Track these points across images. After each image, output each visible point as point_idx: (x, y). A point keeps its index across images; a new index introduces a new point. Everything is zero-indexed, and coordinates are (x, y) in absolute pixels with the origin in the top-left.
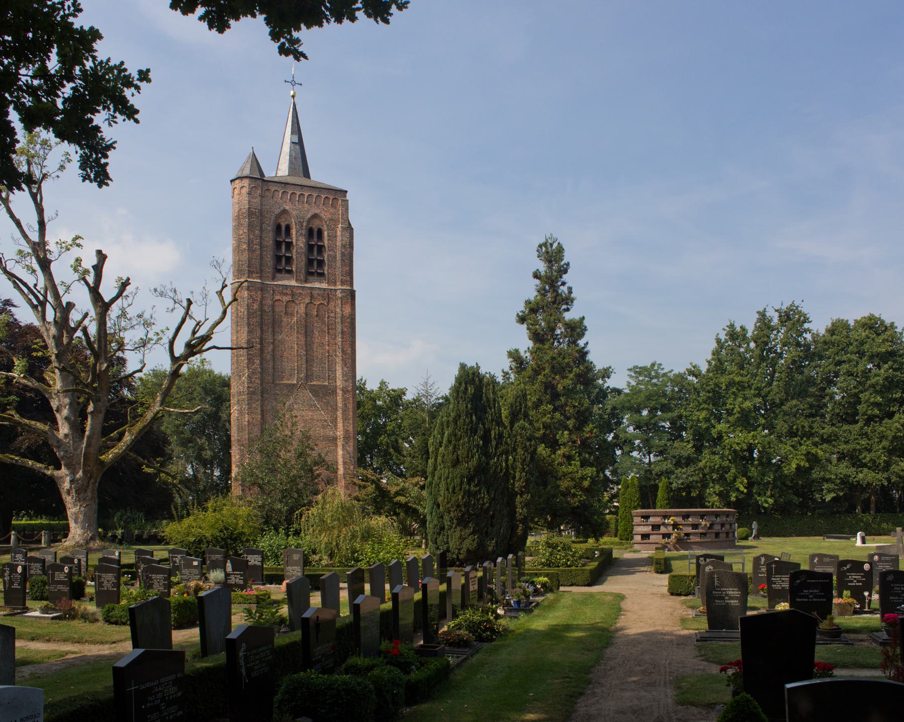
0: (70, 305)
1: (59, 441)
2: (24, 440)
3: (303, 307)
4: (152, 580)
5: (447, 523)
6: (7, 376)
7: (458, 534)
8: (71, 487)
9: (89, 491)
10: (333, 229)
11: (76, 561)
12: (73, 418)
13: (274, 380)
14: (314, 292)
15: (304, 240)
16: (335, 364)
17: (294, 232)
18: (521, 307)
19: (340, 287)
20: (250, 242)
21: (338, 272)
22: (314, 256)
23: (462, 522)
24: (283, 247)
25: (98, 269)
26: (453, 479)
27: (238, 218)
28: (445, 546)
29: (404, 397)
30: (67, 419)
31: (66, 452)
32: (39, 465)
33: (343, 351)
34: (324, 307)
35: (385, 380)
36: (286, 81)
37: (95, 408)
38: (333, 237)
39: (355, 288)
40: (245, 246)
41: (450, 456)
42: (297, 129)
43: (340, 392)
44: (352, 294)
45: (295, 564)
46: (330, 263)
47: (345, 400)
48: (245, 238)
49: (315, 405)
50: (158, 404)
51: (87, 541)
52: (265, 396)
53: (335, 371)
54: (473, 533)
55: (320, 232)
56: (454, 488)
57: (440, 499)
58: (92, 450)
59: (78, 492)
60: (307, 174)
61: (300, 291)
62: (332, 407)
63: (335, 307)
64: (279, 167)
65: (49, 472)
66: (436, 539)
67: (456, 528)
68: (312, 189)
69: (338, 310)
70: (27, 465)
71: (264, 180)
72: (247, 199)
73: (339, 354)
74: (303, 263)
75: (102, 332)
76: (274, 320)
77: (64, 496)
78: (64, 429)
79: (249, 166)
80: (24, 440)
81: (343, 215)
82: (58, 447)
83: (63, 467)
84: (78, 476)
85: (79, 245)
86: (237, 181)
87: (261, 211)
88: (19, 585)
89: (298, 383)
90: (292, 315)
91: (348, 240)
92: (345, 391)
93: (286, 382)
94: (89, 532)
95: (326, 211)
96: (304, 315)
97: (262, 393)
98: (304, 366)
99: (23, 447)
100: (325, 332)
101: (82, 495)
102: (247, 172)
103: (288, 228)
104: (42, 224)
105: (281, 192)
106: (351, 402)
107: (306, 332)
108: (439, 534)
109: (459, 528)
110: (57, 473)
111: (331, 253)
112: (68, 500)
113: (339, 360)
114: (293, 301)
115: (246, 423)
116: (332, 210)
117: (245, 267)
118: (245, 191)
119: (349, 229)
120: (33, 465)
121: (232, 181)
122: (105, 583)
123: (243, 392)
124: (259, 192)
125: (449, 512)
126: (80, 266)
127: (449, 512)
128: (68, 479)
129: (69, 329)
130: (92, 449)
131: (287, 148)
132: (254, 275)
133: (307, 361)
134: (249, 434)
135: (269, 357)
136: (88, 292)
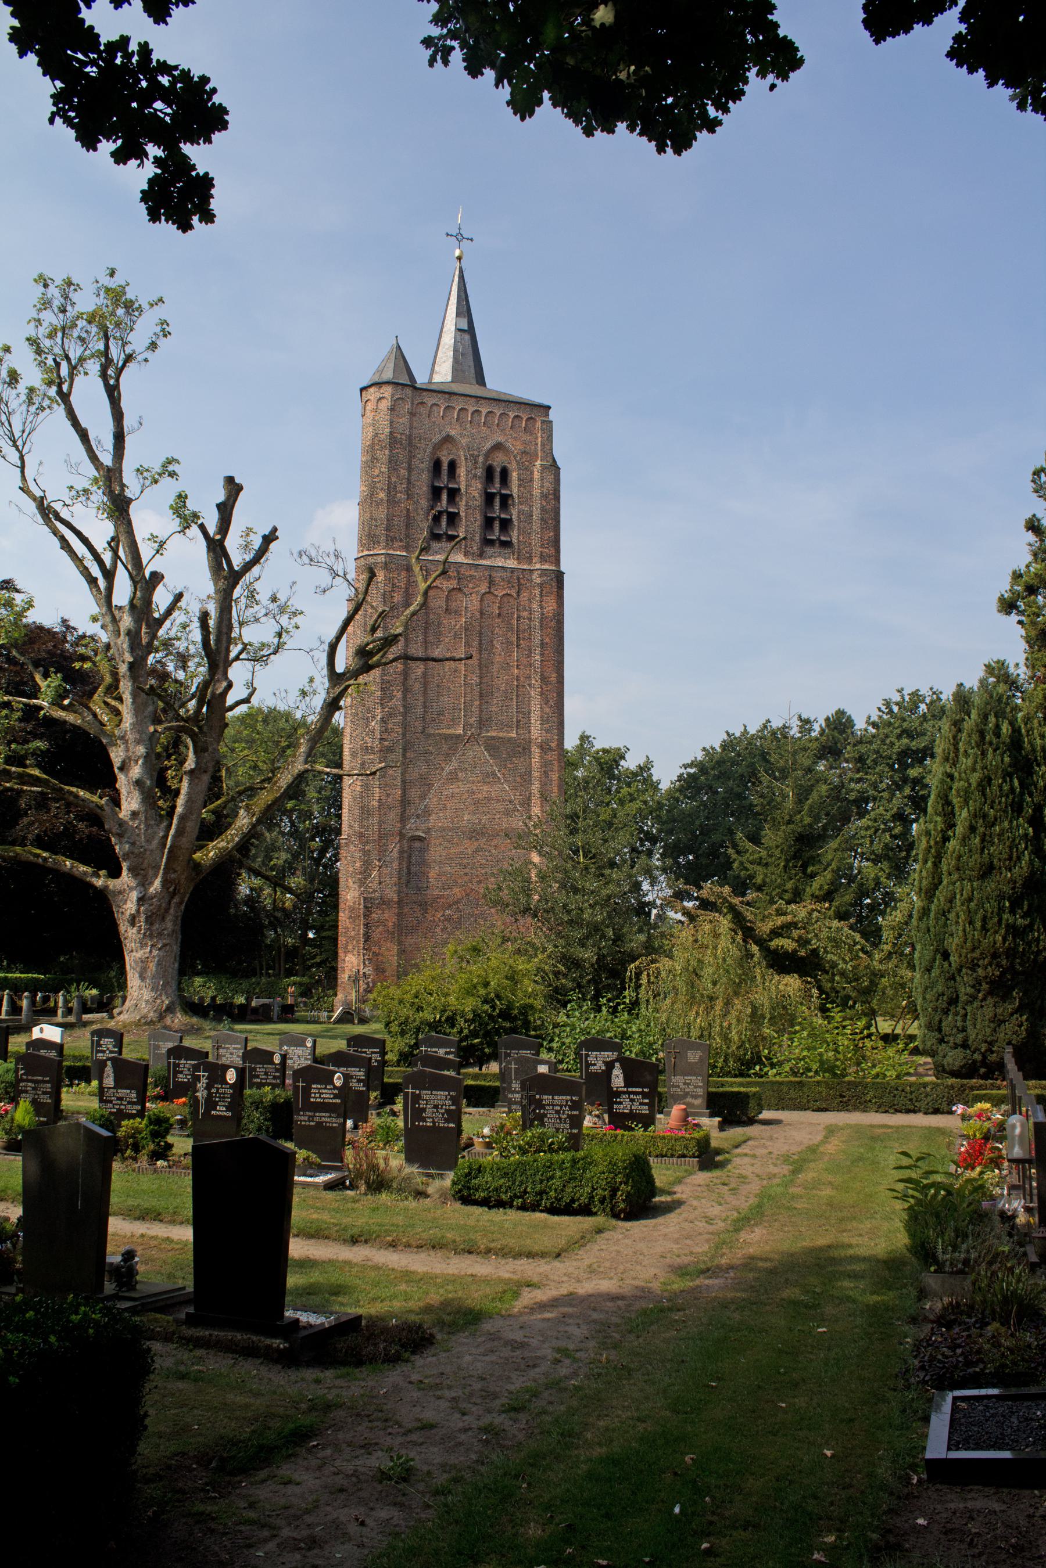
0: (157, 577)
1: (121, 823)
2: (32, 823)
3: (475, 599)
4: (543, 1107)
5: (964, 991)
6: (25, 705)
7: (989, 1012)
8: (138, 911)
9: (169, 918)
10: (526, 469)
11: (277, 1059)
12: (148, 783)
13: (424, 728)
14: (494, 574)
15: (480, 486)
16: (529, 701)
17: (462, 472)
18: (1004, 586)
19: (538, 566)
20: (391, 489)
21: (535, 541)
22: (494, 512)
23: (999, 989)
24: (444, 497)
25: (225, 510)
26: (981, 905)
27: (371, 450)
28: (960, 1036)
29: (622, 763)
30: (138, 783)
31: (133, 844)
32: (83, 868)
33: (543, 678)
34: (512, 600)
35: (587, 733)
36: (448, 235)
37: (197, 763)
38: (526, 482)
39: (562, 569)
40: (382, 495)
41: (977, 856)
42: (465, 309)
43: (536, 751)
44: (559, 578)
45: (690, 1071)
46: (522, 525)
47: (545, 764)
48: (382, 482)
49: (494, 773)
50: (301, 759)
51: (161, 1014)
52: (408, 755)
53: (529, 712)
54: (1019, 1010)
55: (505, 473)
56: (984, 919)
57: (953, 944)
58: (185, 842)
59: (150, 921)
60: (481, 380)
61: (472, 573)
62: (521, 777)
63: (529, 600)
64: (437, 368)
65: (99, 883)
66: (940, 1021)
67: (984, 999)
68: (494, 403)
69: (535, 606)
70: (63, 868)
71: (415, 388)
72: (388, 417)
73: (536, 682)
74: (478, 523)
75: (225, 623)
76: (426, 623)
77: (123, 927)
78: (131, 803)
79: (391, 365)
80: (32, 823)
81: (543, 445)
82: (120, 836)
83: (125, 872)
84: (152, 890)
85: (172, 474)
86: (372, 390)
87: (410, 438)
88: (228, 1109)
89: (465, 733)
90: (458, 613)
91: (551, 487)
92: (545, 748)
93: (444, 731)
94: (164, 998)
95: (515, 439)
96: (477, 614)
97: (405, 750)
98: (477, 703)
99: (30, 836)
100: (512, 644)
101: (156, 926)
102: (388, 375)
103: (453, 466)
104: (119, 438)
105: (443, 407)
106: (556, 768)
107: (480, 644)
108: (946, 1012)
109: (990, 1001)
110: (113, 884)
111: (523, 507)
112: (130, 935)
113: (535, 693)
114: (459, 589)
115: (376, 804)
116: (526, 437)
117: (381, 531)
118: (385, 405)
119: (553, 468)
120: (72, 867)
121: (362, 390)
122: (429, 1112)
123: (372, 747)
124: (408, 406)
125: (974, 967)
126: (185, 506)
127: (974, 967)
128: (134, 895)
129: (151, 621)
130: (184, 840)
131: (448, 339)
132: (396, 544)
133: (481, 695)
134: (381, 822)
135: (417, 686)
136: (205, 549)
